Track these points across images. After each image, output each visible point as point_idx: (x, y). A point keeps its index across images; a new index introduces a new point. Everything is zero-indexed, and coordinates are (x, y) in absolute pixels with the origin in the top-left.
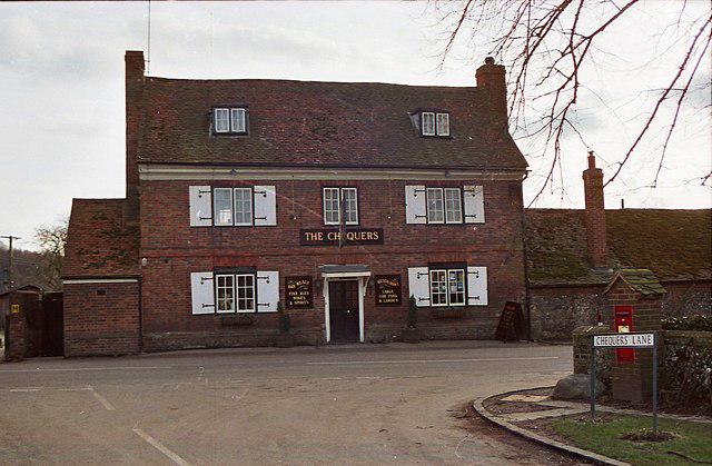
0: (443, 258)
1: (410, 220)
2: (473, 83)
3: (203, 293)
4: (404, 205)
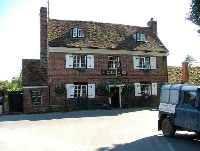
0: (145, 80)
1: (135, 68)
2: (147, 26)
3: (71, 91)
4: (133, 63)
